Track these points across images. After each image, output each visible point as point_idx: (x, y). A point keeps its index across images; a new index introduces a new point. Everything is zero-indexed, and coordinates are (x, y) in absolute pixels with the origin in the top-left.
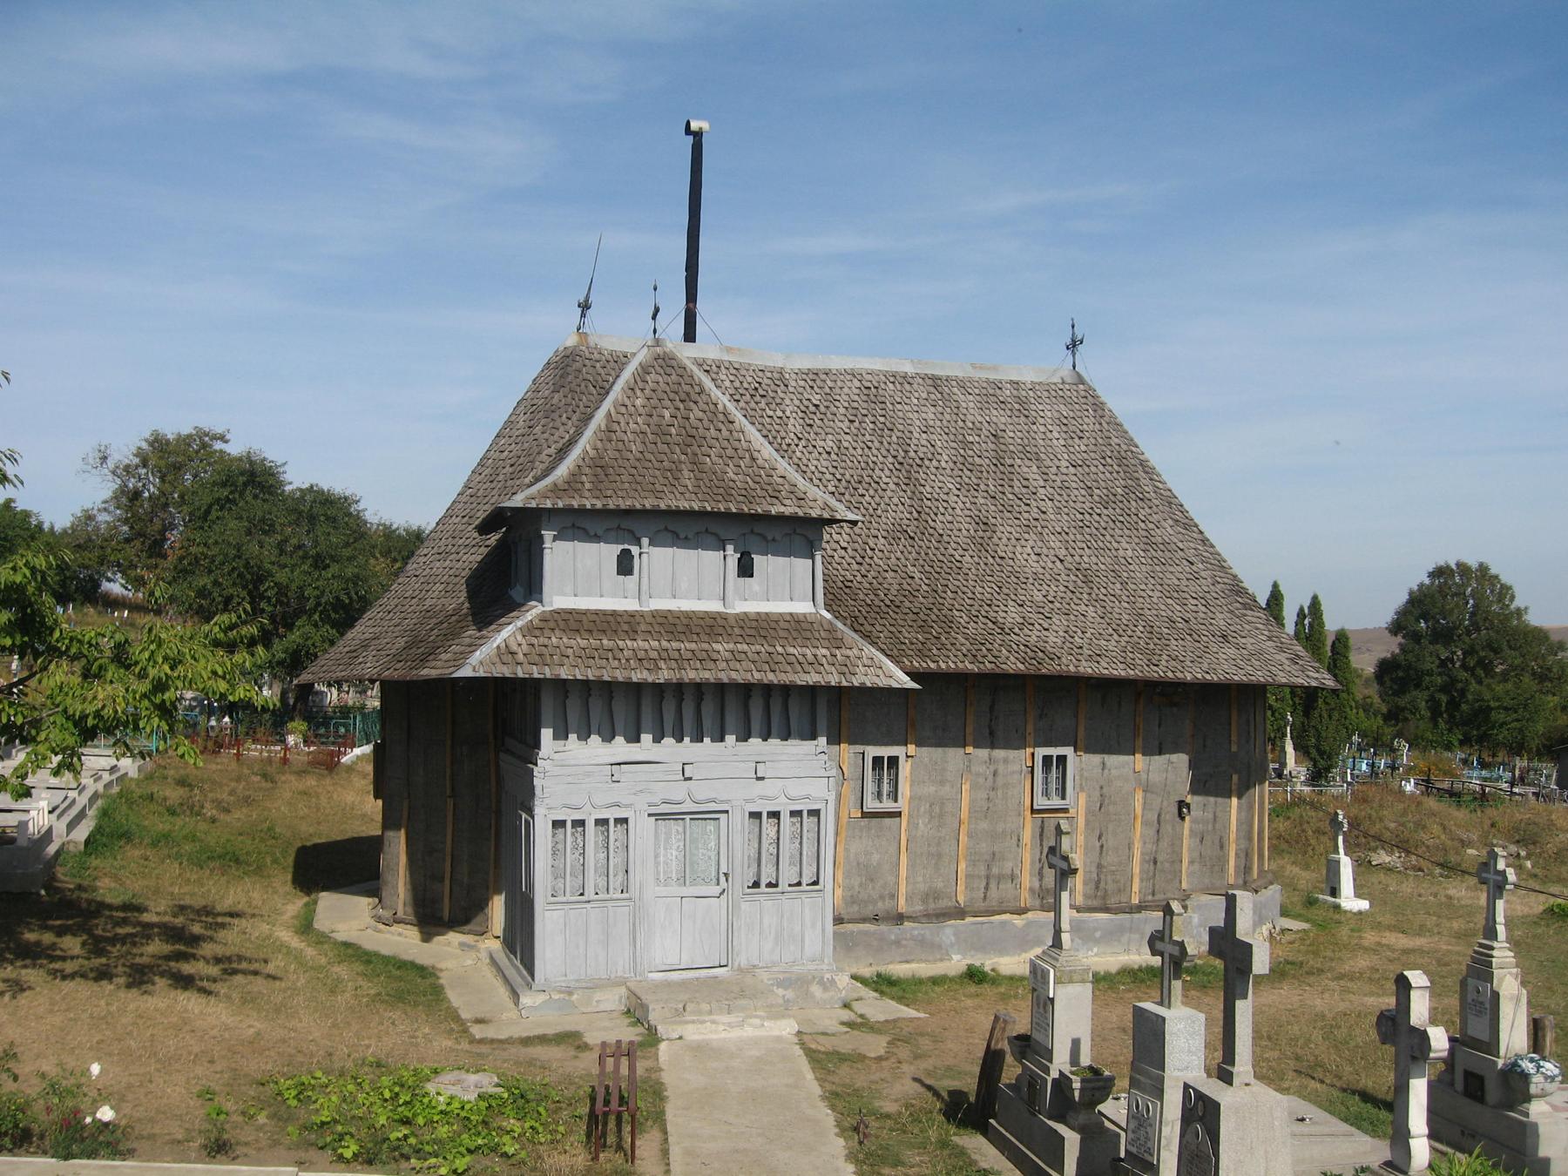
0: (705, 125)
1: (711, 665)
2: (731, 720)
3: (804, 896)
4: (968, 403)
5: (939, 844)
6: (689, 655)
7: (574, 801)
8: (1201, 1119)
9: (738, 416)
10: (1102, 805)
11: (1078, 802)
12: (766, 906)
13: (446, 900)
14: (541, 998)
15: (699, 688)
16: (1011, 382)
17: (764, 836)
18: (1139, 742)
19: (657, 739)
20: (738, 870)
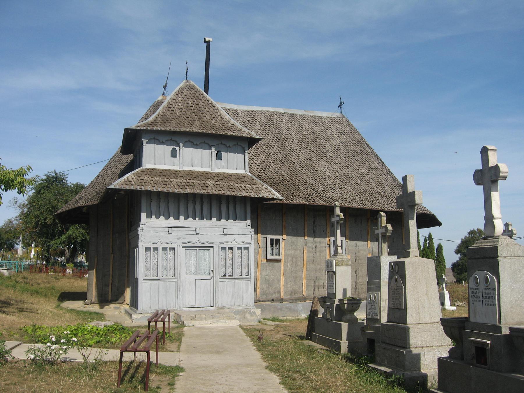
0: (211, 39)
1: (206, 188)
2: (214, 212)
3: (243, 280)
4: (304, 122)
5: (296, 273)
8: (397, 273)
12: (229, 285)
13: (110, 293)
14: (141, 315)
15: (202, 196)
16: (319, 116)
18: (369, 237)
19: (186, 218)
20: (217, 269)
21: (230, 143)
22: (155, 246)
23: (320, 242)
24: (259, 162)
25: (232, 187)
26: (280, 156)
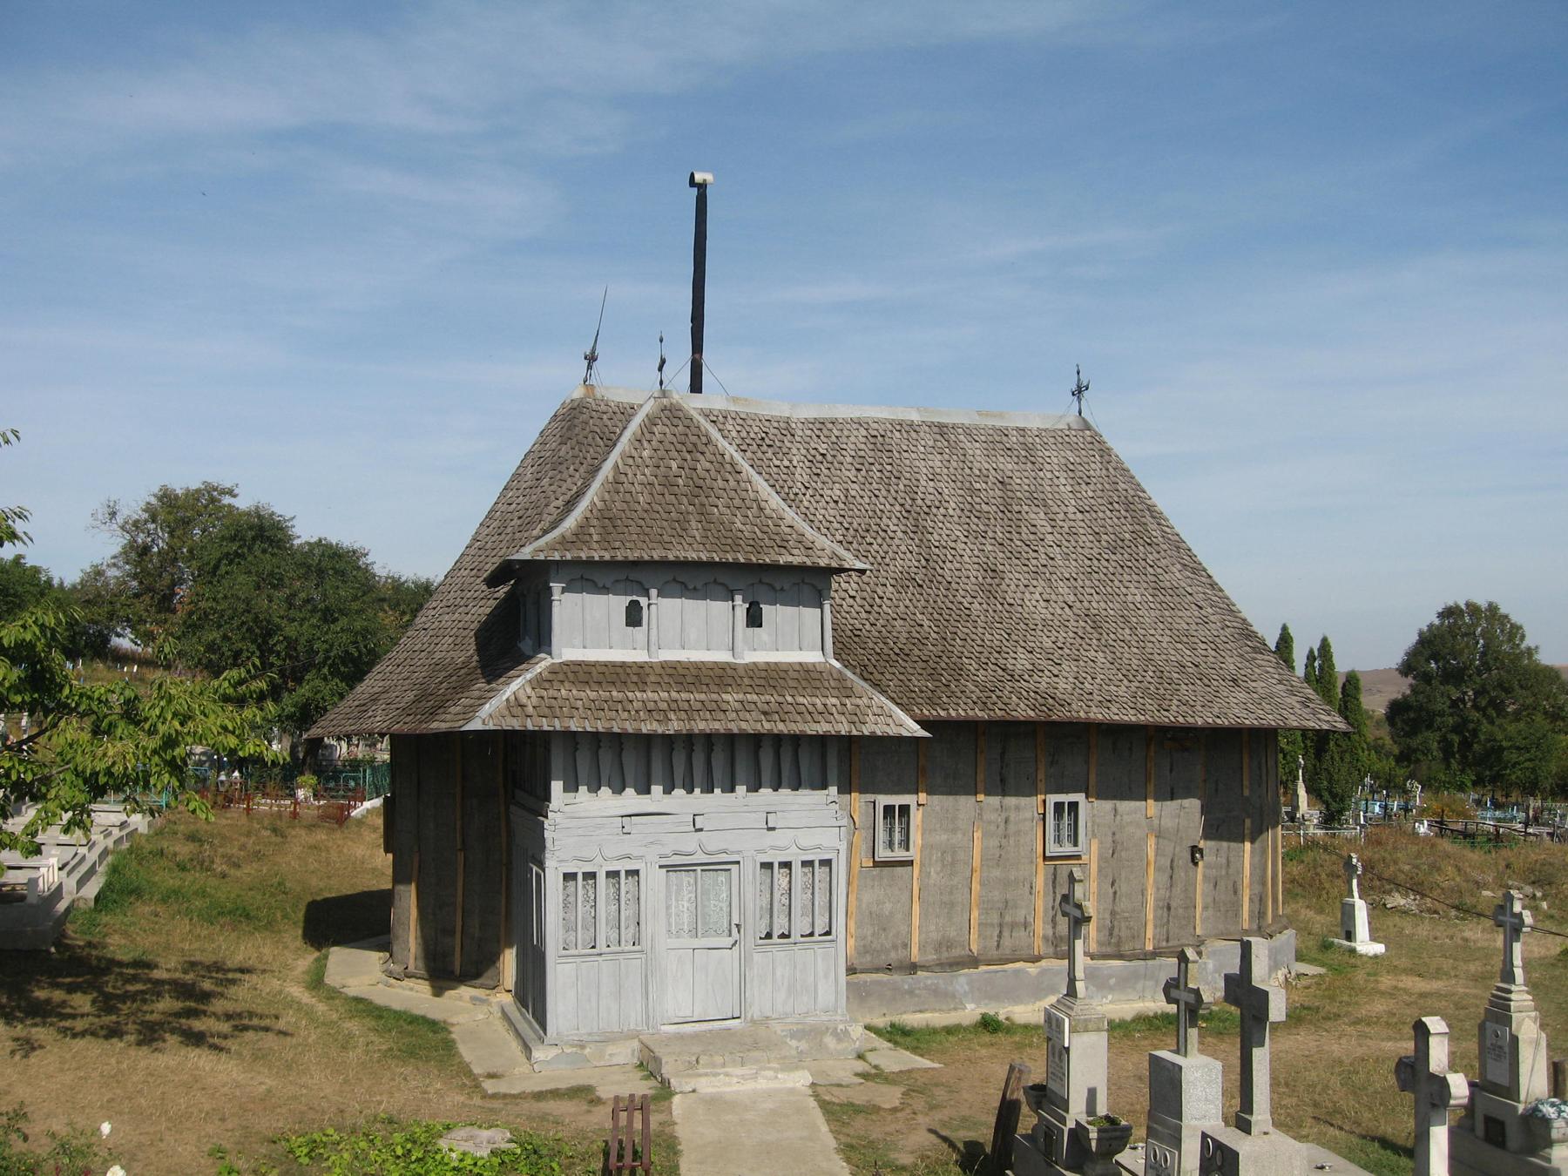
0: (709, 177)
1: (721, 715)
2: (741, 769)
3: (816, 946)
4: (975, 450)
5: (951, 893)
6: (699, 706)
7: (586, 854)
9: (745, 466)
10: (1114, 850)
11: (1090, 849)
14: (554, 1052)
15: (709, 739)
16: (1018, 429)
20: (750, 920)
23: (1017, 808)
24: (855, 586)
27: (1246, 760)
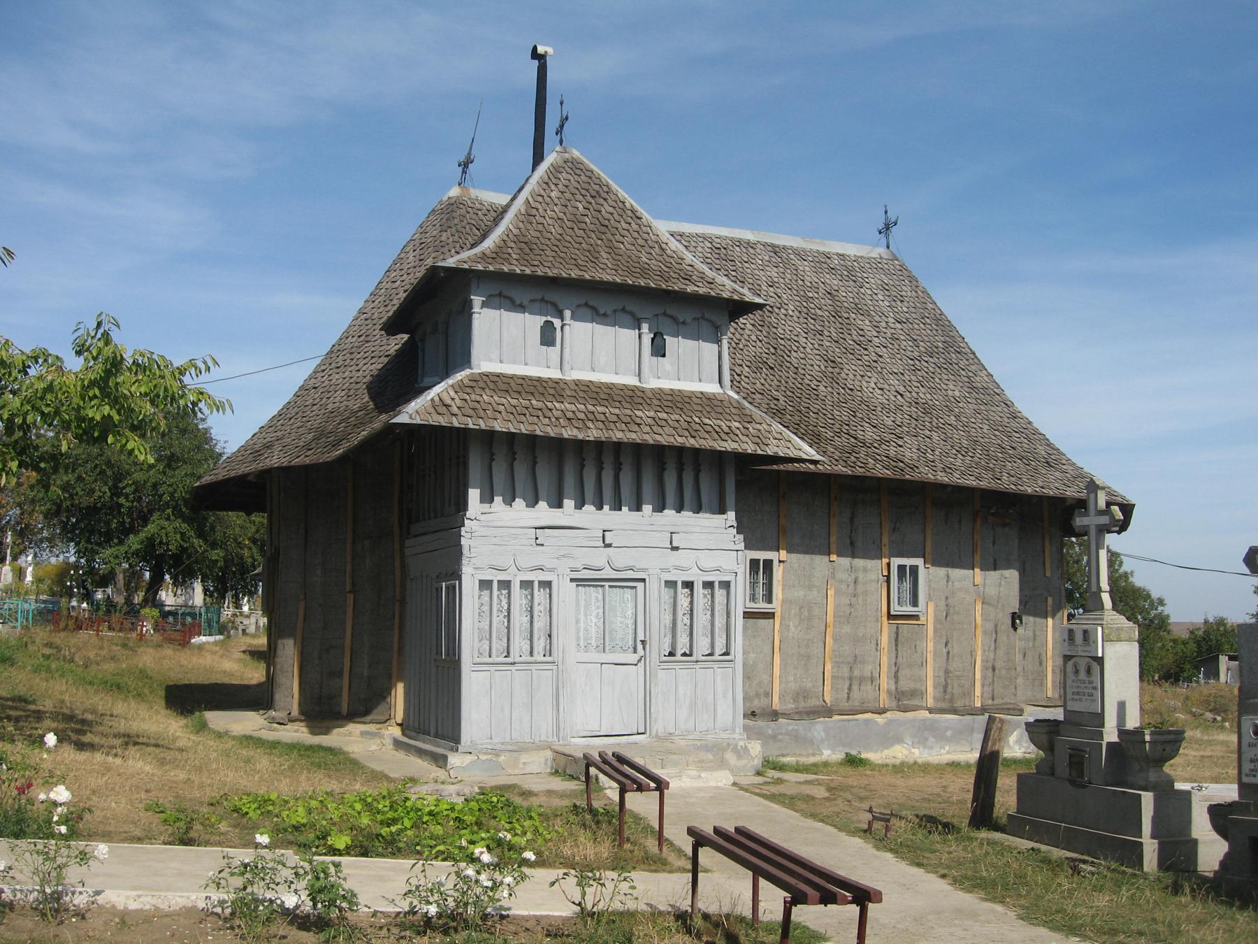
0: (550, 50)
1: (636, 428)
2: (648, 488)
3: (716, 666)
4: (805, 267)
5: (807, 646)
6: (615, 418)
7: (499, 563)
10: (947, 613)
11: (928, 610)
13: (345, 695)
14: (470, 758)
16: (838, 254)
17: (679, 607)
19: (579, 506)
20: (655, 637)
21: (685, 315)
22: (503, 577)
23: (865, 570)
25: (698, 427)
26: (760, 349)
27: (1047, 544)
